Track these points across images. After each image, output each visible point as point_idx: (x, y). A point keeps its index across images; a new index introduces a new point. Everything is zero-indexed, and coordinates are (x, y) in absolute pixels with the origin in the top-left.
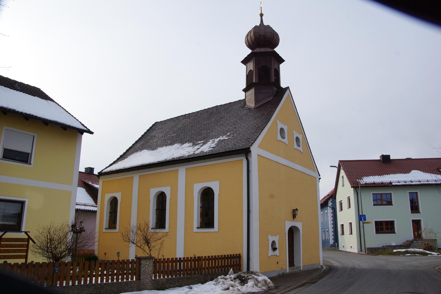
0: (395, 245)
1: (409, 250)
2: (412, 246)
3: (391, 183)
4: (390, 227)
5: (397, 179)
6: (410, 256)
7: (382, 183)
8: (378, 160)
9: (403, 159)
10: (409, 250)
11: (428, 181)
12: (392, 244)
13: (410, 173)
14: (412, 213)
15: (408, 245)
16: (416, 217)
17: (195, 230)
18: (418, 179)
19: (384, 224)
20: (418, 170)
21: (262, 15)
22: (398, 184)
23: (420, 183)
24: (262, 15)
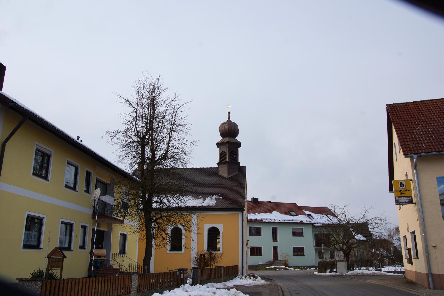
0: (261, 264)
1: (277, 267)
2: (274, 264)
3: (262, 220)
4: (301, 251)
5: (266, 218)
6: (278, 270)
7: (256, 220)
8: (250, 201)
9: (265, 202)
10: (277, 267)
11: (284, 220)
12: (260, 264)
13: (272, 213)
14: (273, 242)
15: (270, 264)
16: (275, 245)
17: (168, 252)
18: (278, 218)
19: (255, 249)
20: (277, 211)
21: (229, 113)
22: (266, 221)
23: (280, 221)
24: (229, 113)
